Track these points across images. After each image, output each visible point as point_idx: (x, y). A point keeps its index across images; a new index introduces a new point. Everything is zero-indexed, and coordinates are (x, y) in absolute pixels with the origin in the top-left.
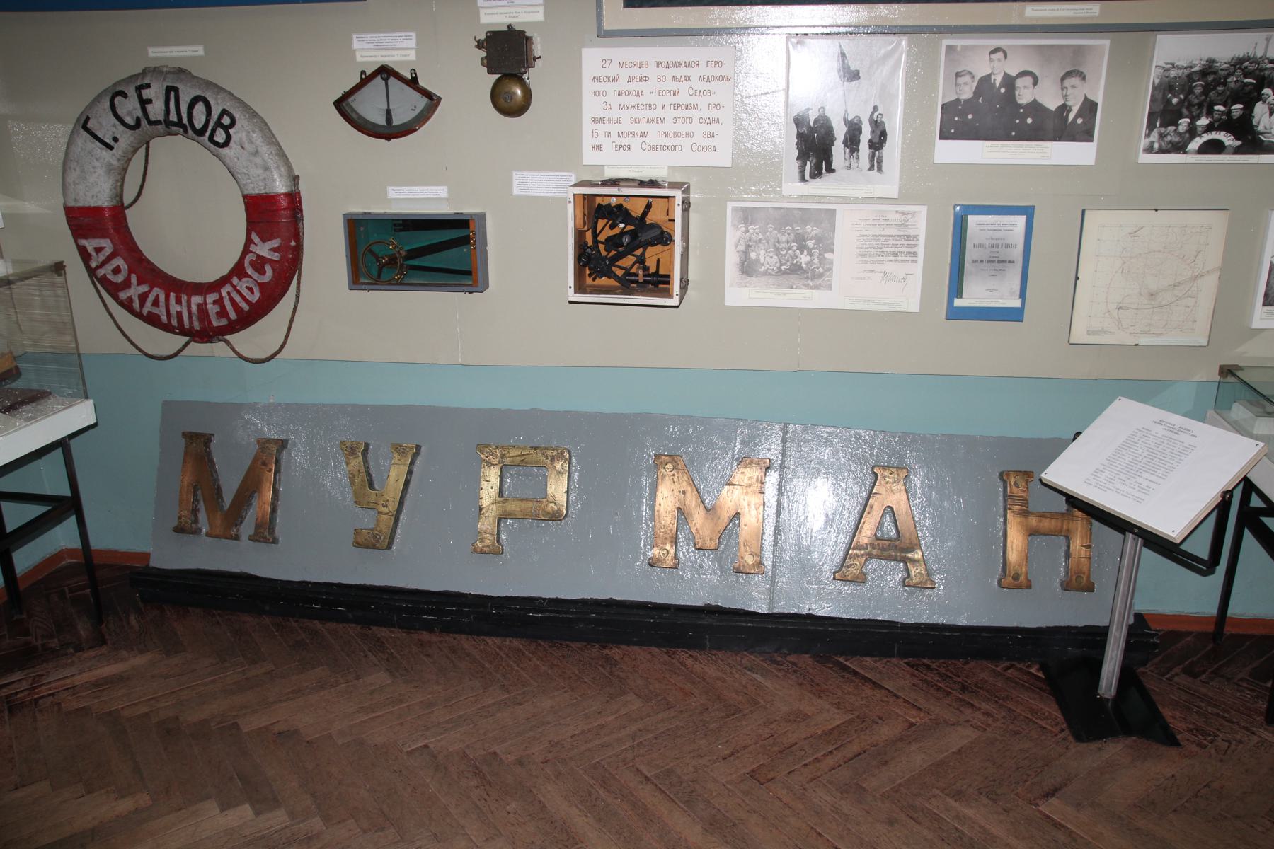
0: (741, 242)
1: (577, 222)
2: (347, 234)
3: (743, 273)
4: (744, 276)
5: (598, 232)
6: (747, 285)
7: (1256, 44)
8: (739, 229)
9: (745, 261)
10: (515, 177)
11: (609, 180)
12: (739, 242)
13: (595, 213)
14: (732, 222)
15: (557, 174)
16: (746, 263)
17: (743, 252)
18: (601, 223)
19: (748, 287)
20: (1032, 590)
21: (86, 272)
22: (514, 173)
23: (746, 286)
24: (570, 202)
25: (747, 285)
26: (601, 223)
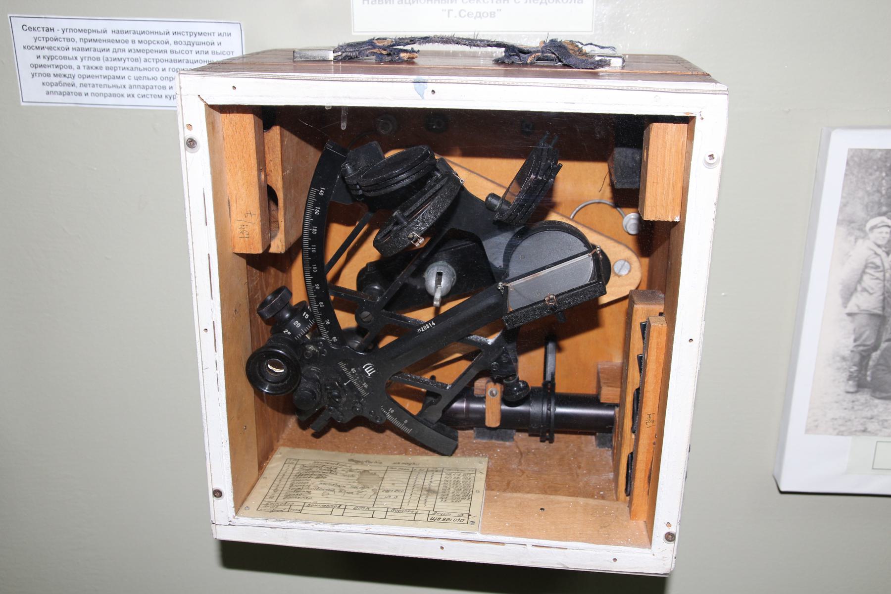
0: (868, 281)
1: (236, 225)
2: (640, 197)
3: (860, 383)
4: (864, 397)
5: (330, 254)
6: (872, 426)
7: (217, 369)
8: (865, 236)
9: (875, 348)
10: (22, 38)
11: (371, 43)
12: (860, 281)
13: (315, 184)
14: (844, 206)
15: (173, 27)
16: (875, 355)
17: (873, 315)
18: (338, 234)
19: (874, 434)
20: (696, 116)
21: (688, 198)
22: (17, 23)
23: (865, 431)
24: (191, 143)
25: (872, 426)
26: (338, 234)
